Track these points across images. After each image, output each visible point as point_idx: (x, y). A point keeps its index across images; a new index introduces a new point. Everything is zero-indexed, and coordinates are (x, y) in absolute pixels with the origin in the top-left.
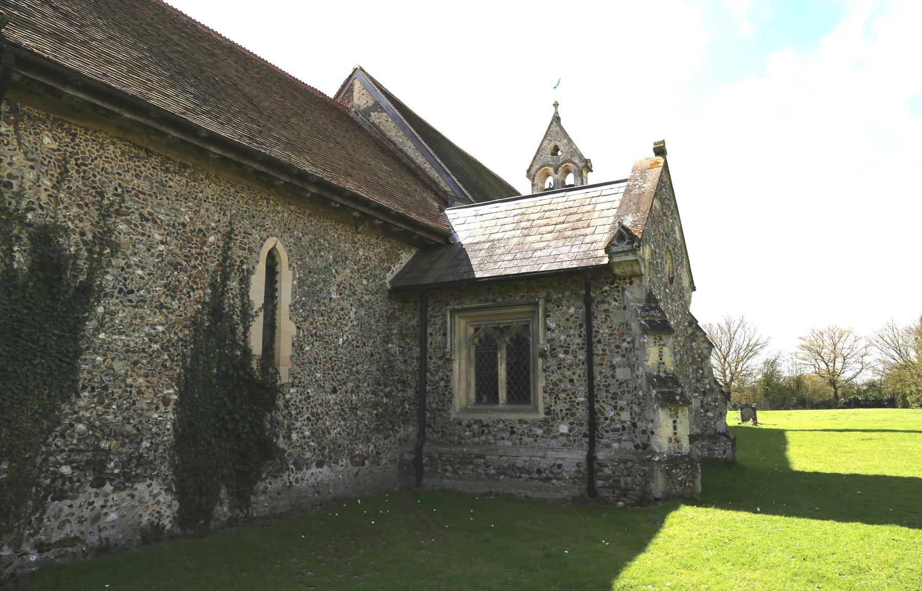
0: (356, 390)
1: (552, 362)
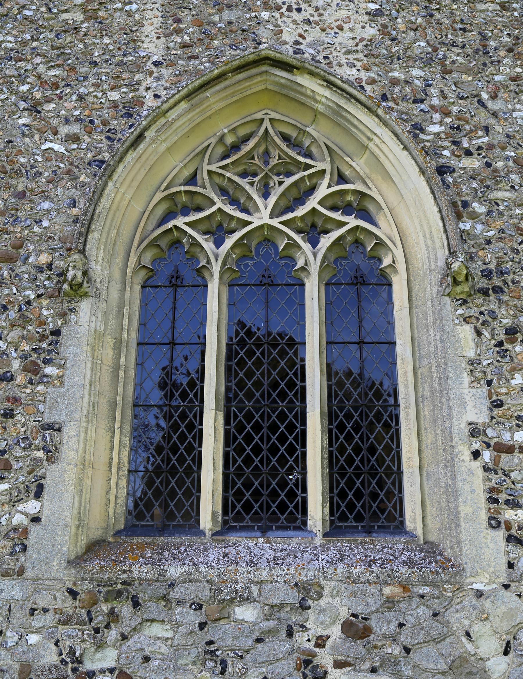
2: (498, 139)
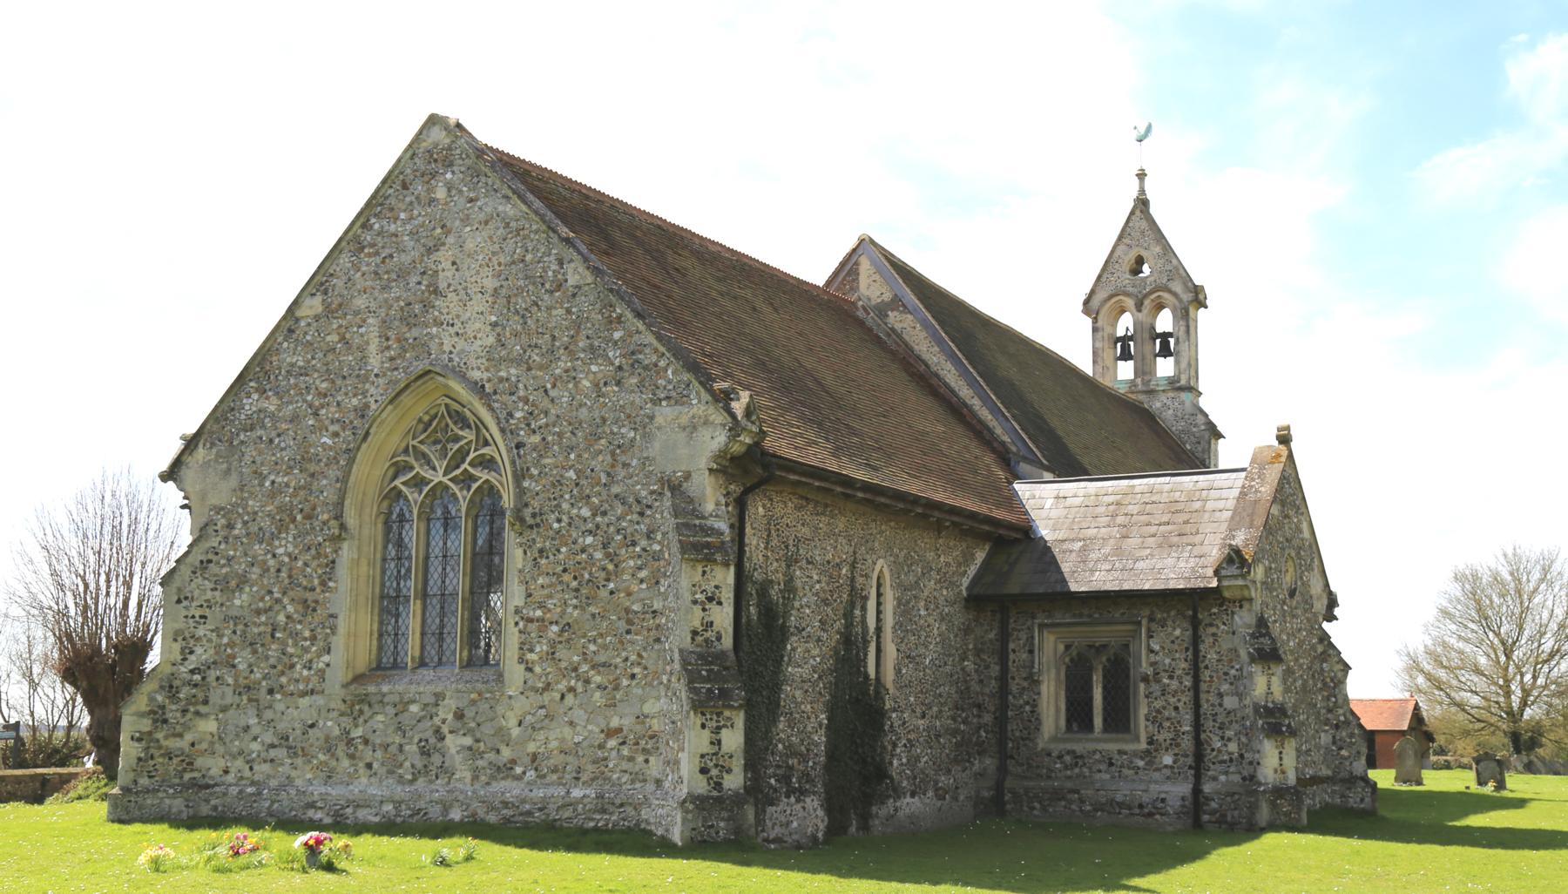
1: (1155, 687)
2: (552, 418)
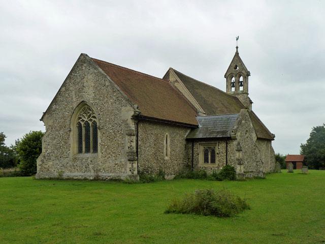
0: (180, 160)
